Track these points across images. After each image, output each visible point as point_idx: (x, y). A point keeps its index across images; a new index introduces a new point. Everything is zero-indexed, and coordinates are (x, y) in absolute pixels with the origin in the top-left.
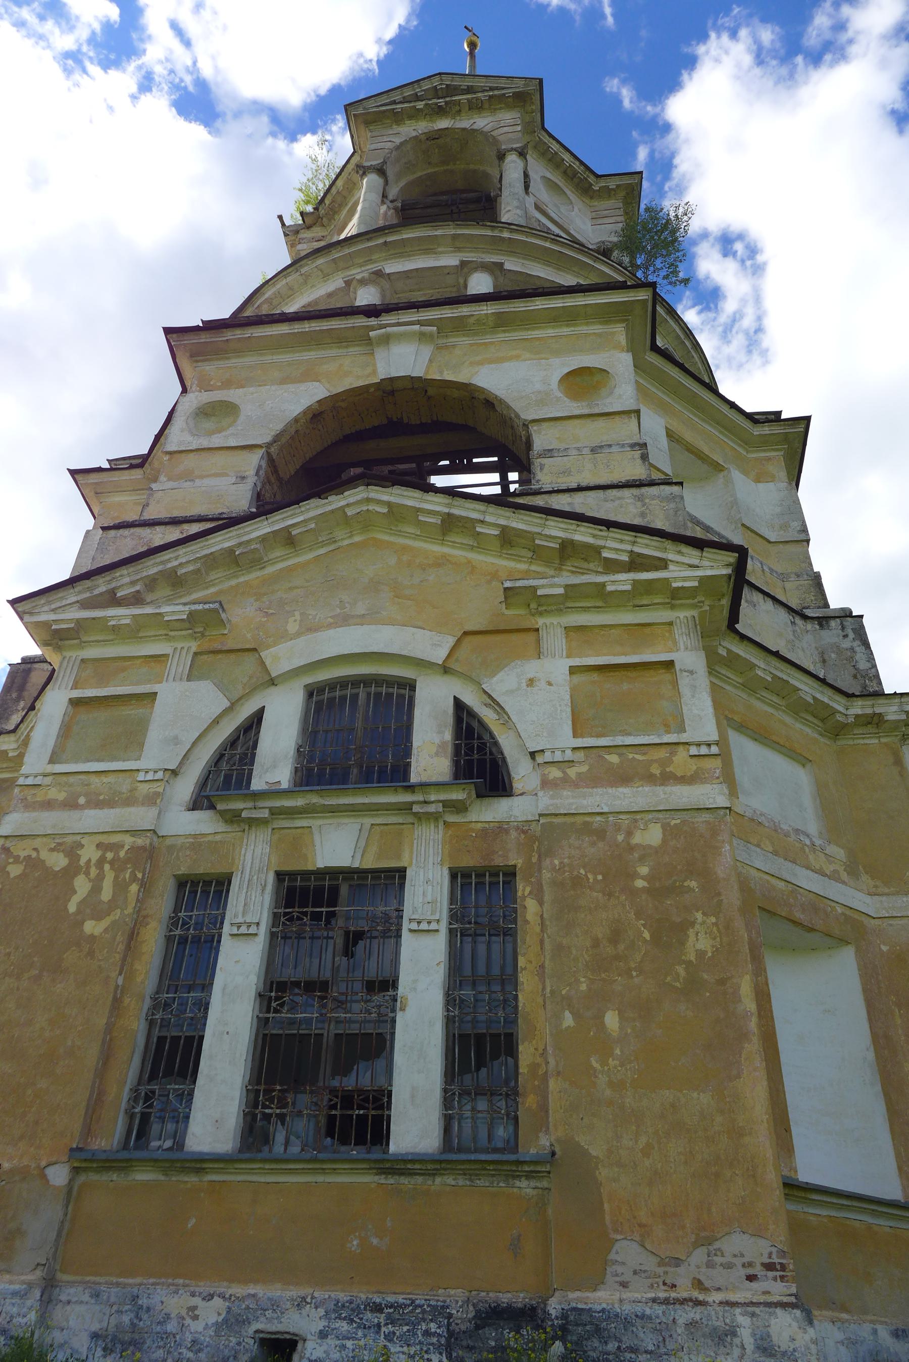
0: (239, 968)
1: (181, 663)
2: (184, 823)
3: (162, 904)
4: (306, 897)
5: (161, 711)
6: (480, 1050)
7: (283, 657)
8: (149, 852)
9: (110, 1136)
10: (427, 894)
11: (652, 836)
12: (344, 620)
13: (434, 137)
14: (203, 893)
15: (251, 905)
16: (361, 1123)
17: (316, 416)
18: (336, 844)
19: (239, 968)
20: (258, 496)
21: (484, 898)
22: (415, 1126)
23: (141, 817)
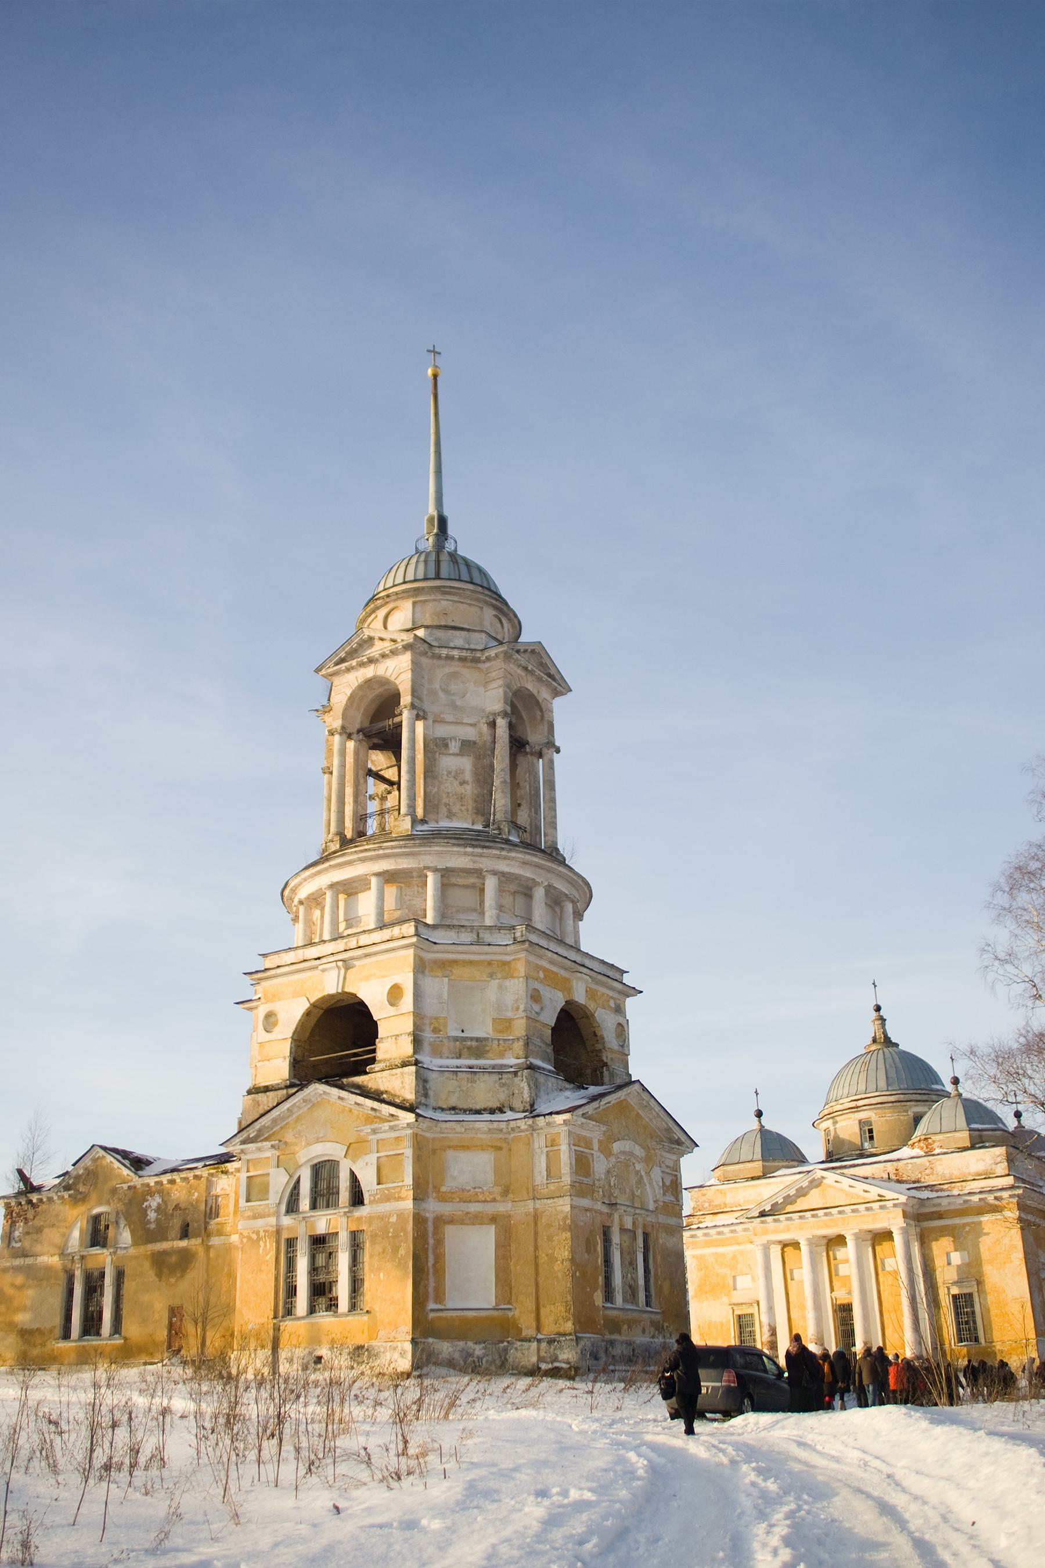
0: (302, 1264)
4: (319, 1242)
10: (344, 1238)
11: (394, 1219)
12: (318, 1140)
13: (368, 683)
16: (332, 1305)
17: (308, 1014)
18: (321, 1229)
19: (302, 1264)
20: (296, 1064)
22: (343, 1304)
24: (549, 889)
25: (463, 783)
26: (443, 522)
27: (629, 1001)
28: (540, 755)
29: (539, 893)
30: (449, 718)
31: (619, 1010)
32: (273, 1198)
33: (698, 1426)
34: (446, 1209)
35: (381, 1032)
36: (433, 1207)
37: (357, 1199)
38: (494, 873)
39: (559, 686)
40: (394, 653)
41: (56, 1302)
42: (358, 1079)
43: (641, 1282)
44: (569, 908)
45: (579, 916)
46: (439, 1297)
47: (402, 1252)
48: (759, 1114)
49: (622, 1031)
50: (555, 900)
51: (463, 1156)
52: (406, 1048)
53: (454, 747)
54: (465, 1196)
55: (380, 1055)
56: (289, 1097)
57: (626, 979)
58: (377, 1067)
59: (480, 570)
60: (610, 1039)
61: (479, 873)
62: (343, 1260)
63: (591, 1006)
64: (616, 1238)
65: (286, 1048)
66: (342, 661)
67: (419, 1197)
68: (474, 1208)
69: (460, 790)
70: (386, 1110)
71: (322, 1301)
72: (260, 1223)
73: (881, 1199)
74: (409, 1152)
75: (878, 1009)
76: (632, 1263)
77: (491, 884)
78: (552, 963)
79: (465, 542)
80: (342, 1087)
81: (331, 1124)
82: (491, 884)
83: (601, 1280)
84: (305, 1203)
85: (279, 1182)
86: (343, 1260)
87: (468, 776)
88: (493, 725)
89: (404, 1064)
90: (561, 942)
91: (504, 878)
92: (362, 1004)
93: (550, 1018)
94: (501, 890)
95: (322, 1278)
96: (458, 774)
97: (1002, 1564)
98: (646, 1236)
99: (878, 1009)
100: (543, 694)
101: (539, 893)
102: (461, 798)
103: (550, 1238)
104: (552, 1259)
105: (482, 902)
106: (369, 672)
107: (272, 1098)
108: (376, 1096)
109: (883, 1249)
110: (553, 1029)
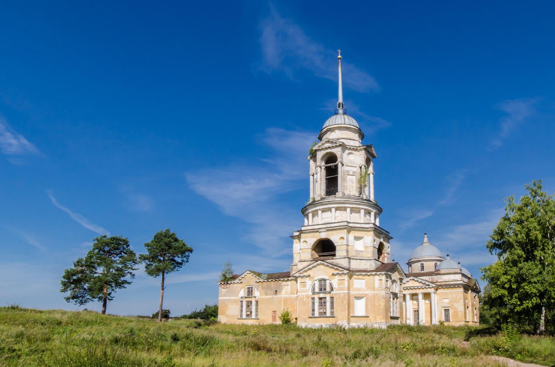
0: (317, 304)
5: (307, 283)
7: (316, 278)
12: (320, 275)
13: (327, 153)
15: (317, 300)
17: (315, 242)
18: (322, 295)
19: (317, 304)
21: (332, 298)
22: (328, 314)
25: (353, 183)
30: (350, 165)
35: (337, 248)
37: (332, 289)
40: (336, 146)
46: (353, 313)
52: (345, 254)
54: (359, 289)
55: (337, 255)
57: (390, 235)
67: (349, 289)
68: (361, 292)
84: (317, 290)
87: (354, 181)
88: (361, 168)
89: (344, 258)
91: (365, 210)
96: (352, 180)
103: (379, 300)
104: (380, 305)
106: (329, 151)
107: (306, 264)
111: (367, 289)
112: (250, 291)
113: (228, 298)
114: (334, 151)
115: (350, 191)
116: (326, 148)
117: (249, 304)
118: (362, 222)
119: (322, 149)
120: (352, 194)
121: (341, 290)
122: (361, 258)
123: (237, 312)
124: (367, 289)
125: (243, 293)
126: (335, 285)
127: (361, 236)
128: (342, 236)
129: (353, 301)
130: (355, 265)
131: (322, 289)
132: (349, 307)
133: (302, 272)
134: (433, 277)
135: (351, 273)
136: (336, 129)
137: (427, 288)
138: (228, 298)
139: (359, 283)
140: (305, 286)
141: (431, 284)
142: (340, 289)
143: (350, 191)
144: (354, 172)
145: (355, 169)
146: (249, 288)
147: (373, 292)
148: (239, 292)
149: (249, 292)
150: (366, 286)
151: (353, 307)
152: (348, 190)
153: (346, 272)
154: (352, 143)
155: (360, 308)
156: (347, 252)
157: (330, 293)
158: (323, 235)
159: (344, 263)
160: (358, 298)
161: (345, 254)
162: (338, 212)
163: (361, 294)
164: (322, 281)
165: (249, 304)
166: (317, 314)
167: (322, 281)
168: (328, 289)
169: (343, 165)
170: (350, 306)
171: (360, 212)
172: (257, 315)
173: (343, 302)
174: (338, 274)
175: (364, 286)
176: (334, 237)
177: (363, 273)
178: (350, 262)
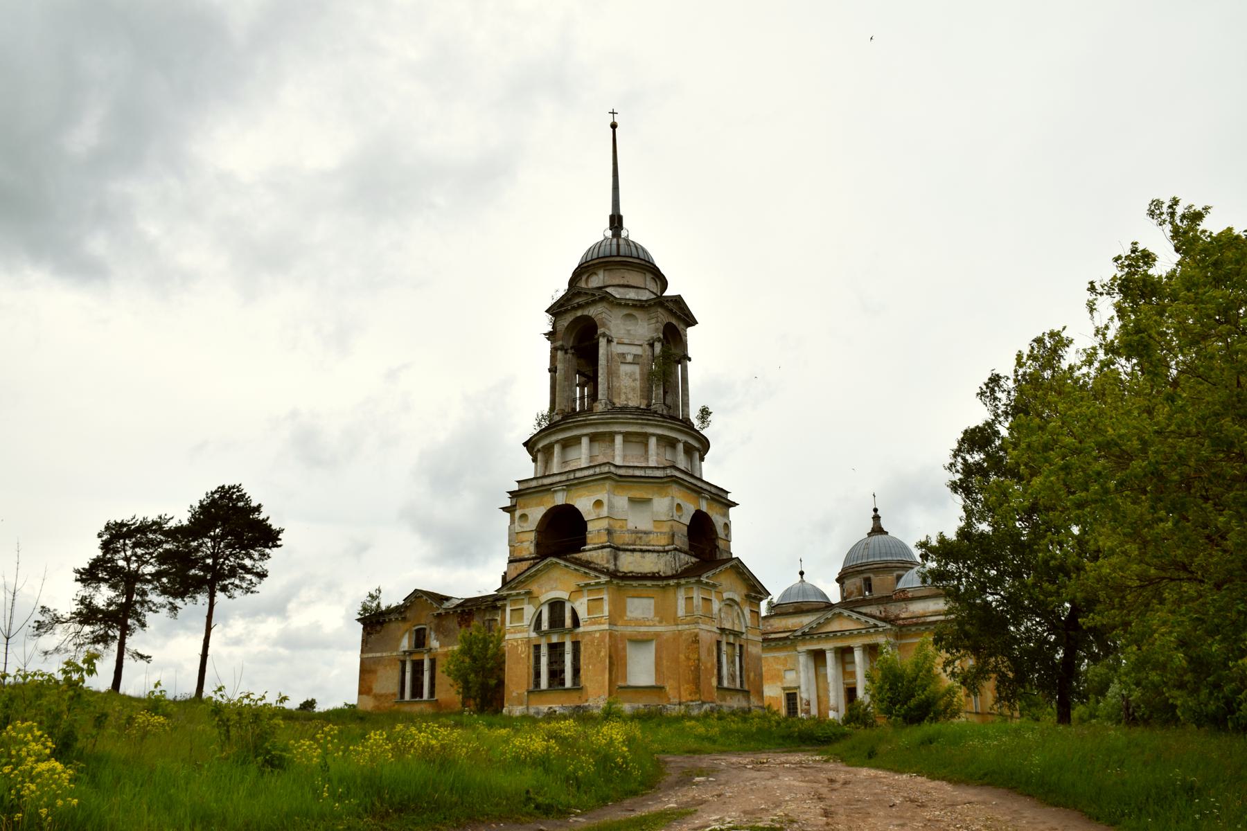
0: (544, 661)
1: (526, 601)
2: (533, 635)
3: (532, 650)
6: (576, 671)
7: (544, 598)
8: (529, 640)
9: (532, 687)
11: (597, 635)
12: (552, 589)
14: (537, 647)
15: (544, 650)
16: (562, 682)
17: (545, 516)
19: (544, 661)
21: (576, 645)
22: (568, 683)
23: (526, 635)
24: (686, 444)
25: (635, 380)
26: (620, 218)
27: (731, 510)
28: (679, 362)
29: (680, 446)
30: (626, 341)
31: (726, 515)
32: (526, 622)
33: (254, 504)
34: (629, 630)
35: (590, 527)
36: (620, 629)
38: (653, 435)
39: (691, 321)
40: (594, 302)
41: (395, 674)
42: (576, 555)
43: (738, 673)
44: (697, 455)
45: (702, 459)
46: (625, 678)
47: (602, 654)
48: (802, 573)
49: (727, 526)
50: (689, 450)
51: (636, 601)
52: (604, 539)
53: (629, 358)
54: (638, 622)
56: (534, 565)
57: (730, 497)
58: (587, 547)
59: (643, 250)
60: (721, 532)
61: (647, 436)
62: (568, 659)
63: (710, 513)
64: (724, 647)
65: (532, 536)
66: (562, 305)
68: (643, 629)
69: (633, 384)
70: (592, 573)
71: (557, 681)
72: (519, 636)
73: (876, 626)
74: (606, 597)
75: (876, 510)
76: (733, 662)
77: (653, 441)
78: (688, 488)
79: (633, 230)
80: (566, 560)
81: (558, 584)
82: (653, 441)
83: (715, 671)
84: (545, 626)
85: (529, 611)
86: (568, 659)
87: (638, 376)
90: (692, 476)
91: (660, 438)
92: (577, 510)
93: (687, 520)
94: (658, 444)
95: (555, 667)
96: (631, 375)
97: (178, 698)
98: (741, 646)
99: (876, 510)
100: (680, 326)
101: (680, 446)
102: (634, 389)
105: (647, 451)
106: (579, 313)
107: (524, 565)
108: (587, 564)
109: (848, 658)
110: (689, 527)
111: (660, 622)
112: (420, 640)
113: (378, 655)
114: (592, 312)
115: (627, 399)
116: (574, 309)
117: (418, 667)
118: (652, 464)
119: (566, 311)
120: (631, 404)
121: (594, 624)
122: (645, 548)
123: (393, 687)
124: (660, 622)
125: (406, 644)
126: (582, 614)
127: (645, 496)
128: (598, 497)
129: (624, 649)
130: (628, 563)
131: (557, 620)
132: (611, 663)
133: (513, 585)
134: (888, 606)
135: (620, 579)
136: (599, 268)
137: (871, 634)
138: (378, 655)
139: (640, 608)
140: (521, 618)
141: (880, 624)
142: (594, 622)
143: (627, 399)
144: (635, 356)
145: (638, 351)
146: (418, 631)
147: (674, 628)
148: (399, 640)
149: (417, 639)
150: (657, 613)
151: (625, 665)
152: (623, 397)
153: (603, 579)
154: (632, 295)
155: (641, 669)
156: (610, 532)
157: (570, 631)
158: (560, 499)
159: (601, 558)
160: (640, 641)
161: (604, 539)
162: (596, 445)
163: (645, 633)
164: (557, 607)
165: (418, 667)
166: (544, 684)
167: (557, 607)
168: (568, 622)
169: (609, 341)
170: (616, 663)
171: (613, 441)
172: (432, 693)
173: (599, 652)
174: (587, 585)
175: (651, 614)
176: (583, 503)
177: (649, 583)
178: (616, 558)
